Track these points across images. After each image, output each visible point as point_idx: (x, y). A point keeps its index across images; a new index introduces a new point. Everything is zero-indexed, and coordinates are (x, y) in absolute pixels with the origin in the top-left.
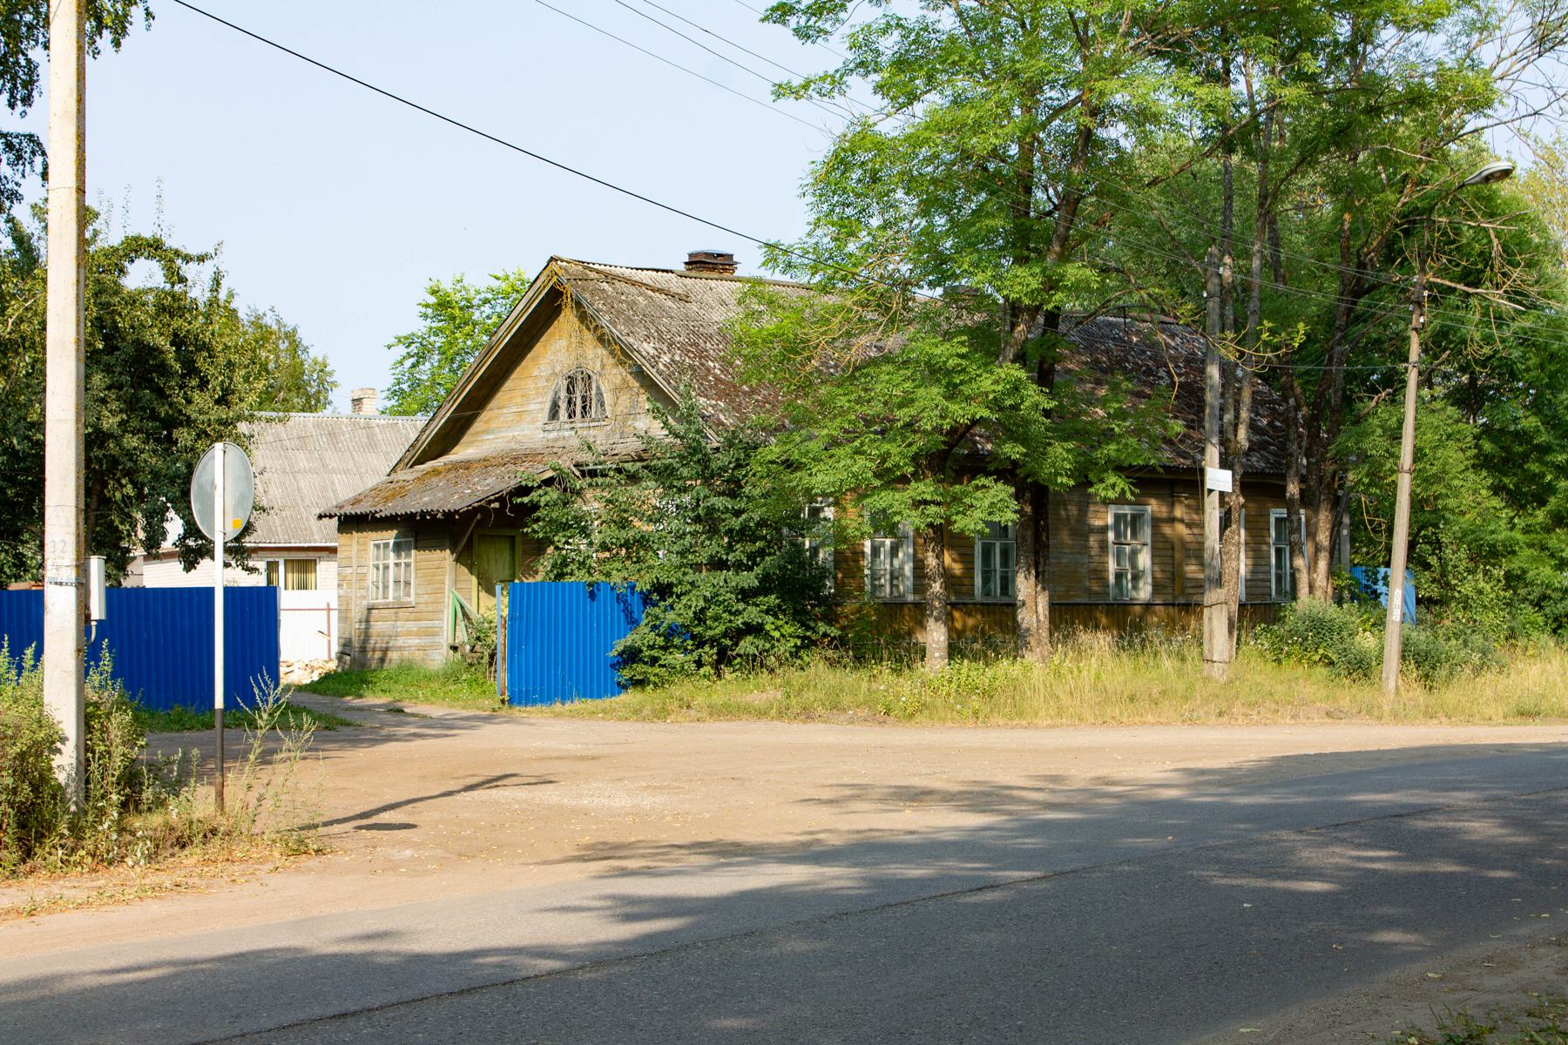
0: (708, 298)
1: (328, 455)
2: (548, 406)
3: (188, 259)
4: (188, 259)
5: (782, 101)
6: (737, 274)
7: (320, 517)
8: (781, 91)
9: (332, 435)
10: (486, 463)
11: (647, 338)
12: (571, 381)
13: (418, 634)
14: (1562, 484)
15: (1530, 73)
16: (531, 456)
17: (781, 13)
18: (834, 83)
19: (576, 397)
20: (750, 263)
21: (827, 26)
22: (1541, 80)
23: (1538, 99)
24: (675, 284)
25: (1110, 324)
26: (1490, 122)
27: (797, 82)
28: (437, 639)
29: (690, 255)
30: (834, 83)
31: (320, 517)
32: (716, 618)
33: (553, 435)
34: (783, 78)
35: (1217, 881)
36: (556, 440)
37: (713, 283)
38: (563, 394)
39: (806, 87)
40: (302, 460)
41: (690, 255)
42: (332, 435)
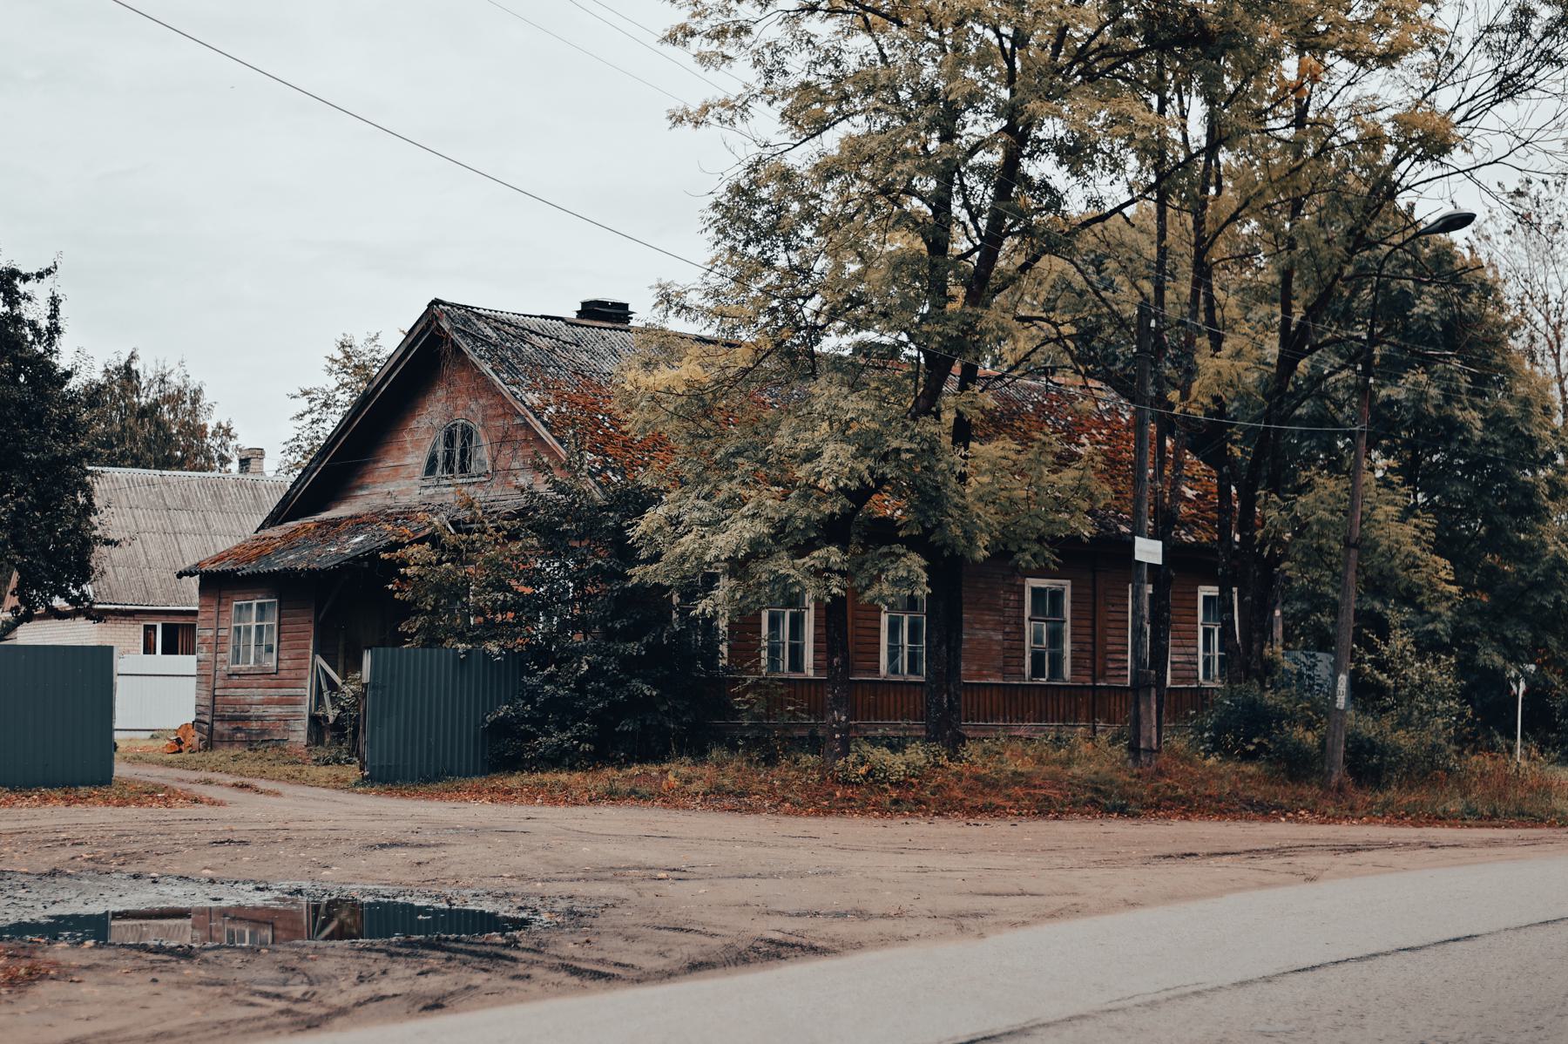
0: (601, 348)
1: (211, 516)
2: (424, 463)
3: (26, 278)
4: (26, 278)
5: (679, 129)
6: (632, 323)
7: (180, 575)
8: (677, 119)
9: (217, 496)
10: (358, 523)
11: (532, 389)
12: (450, 439)
13: (279, 703)
14: (1144, 3)
15: (1489, 120)
16: (407, 514)
17: (680, 35)
18: (737, 108)
19: (454, 455)
20: (643, 313)
21: (730, 52)
22: (1503, 127)
23: (1501, 145)
24: (566, 333)
25: (1029, 387)
26: (1439, 172)
27: (695, 106)
28: (299, 708)
29: (584, 304)
30: (737, 108)
31: (180, 575)
32: (598, 693)
33: (431, 491)
34: (676, 105)
35: (366, 678)
36: (432, 497)
37: (606, 333)
38: (441, 449)
39: (705, 109)
40: (184, 521)
41: (584, 304)
42: (217, 496)
